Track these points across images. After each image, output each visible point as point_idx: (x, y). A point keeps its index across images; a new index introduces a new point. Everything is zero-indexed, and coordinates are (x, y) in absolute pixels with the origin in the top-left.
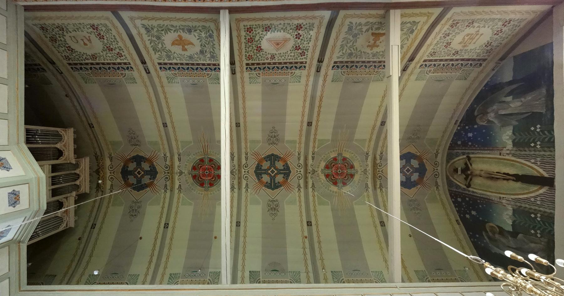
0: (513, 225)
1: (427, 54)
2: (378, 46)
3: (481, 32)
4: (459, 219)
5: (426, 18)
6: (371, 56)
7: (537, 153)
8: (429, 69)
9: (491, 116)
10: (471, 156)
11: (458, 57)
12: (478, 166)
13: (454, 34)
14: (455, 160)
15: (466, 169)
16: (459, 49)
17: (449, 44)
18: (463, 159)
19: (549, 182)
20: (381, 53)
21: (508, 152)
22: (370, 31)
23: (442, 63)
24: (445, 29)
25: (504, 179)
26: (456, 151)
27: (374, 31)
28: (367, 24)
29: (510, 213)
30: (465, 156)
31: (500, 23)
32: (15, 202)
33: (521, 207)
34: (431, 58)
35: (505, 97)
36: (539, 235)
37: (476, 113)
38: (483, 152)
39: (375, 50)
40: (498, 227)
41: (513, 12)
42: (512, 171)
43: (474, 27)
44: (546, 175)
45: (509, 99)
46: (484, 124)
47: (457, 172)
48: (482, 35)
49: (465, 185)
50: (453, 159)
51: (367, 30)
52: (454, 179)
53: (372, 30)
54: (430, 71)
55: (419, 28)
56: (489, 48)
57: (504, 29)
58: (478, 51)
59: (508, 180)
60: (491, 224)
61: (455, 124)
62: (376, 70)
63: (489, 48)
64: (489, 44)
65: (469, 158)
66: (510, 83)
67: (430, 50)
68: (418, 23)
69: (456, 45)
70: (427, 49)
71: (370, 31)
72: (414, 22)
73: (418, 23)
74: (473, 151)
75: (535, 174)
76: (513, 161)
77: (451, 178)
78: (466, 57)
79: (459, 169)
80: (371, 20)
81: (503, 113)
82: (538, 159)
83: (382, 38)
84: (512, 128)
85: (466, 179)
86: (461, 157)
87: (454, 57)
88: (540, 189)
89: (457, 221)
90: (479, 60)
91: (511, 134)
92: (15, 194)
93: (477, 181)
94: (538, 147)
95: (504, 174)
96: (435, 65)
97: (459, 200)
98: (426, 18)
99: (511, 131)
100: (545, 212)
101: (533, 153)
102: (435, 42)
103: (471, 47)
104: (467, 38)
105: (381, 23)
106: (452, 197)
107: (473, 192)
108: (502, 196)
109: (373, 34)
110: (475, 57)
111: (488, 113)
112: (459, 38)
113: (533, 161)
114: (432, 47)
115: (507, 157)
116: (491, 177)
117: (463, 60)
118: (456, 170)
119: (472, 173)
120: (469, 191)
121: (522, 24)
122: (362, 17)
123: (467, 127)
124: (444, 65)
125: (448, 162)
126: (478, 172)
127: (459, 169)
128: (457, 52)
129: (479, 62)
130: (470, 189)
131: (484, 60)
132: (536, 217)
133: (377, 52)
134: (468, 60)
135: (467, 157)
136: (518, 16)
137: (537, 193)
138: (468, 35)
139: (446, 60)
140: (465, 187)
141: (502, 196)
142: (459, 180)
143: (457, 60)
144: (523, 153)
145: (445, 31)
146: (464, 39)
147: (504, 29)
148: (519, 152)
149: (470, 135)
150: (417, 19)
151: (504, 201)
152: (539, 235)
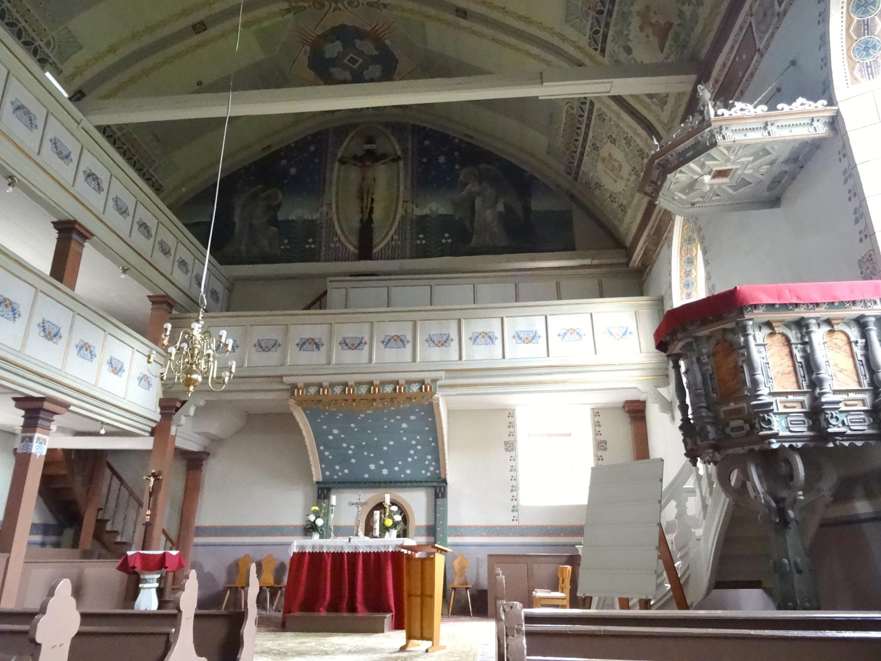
0: (288, 222)
1: (604, 109)
2: (642, 28)
3: (619, 181)
4: (274, 149)
5: (665, 121)
6: (625, 9)
7: (408, 241)
8: (575, 106)
9: (473, 187)
10: (401, 164)
11: (587, 149)
12: (381, 173)
13: (627, 150)
14: (392, 138)
15: (372, 157)
16: (600, 152)
17: (614, 142)
18: (394, 149)
19: (365, 251)
20: (625, 32)
21: (409, 210)
22: (677, 21)
23: (583, 127)
24: (639, 141)
25: (362, 208)
26: (410, 138)
27: (675, 28)
28: (695, 17)
29: (308, 217)
30: (399, 153)
31: (625, 203)
32: (44, 330)
33: (321, 228)
34: (595, 114)
35: (504, 203)
36: (282, 247)
37: (483, 166)
38: (409, 182)
39: (635, 22)
40: (280, 203)
41: (635, 217)
42: (377, 215)
43: (630, 175)
44: (375, 251)
45: (501, 207)
46: (461, 177)
47: (367, 143)
48: (616, 181)
49: (343, 157)
50: (393, 134)
51: (681, 15)
52: (353, 138)
53: (679, 25)
54: (572, 108)
55: (653, 107)
56: (592, 185)
57: (616, 205)
58: (591, 175)
59: (362, 212)
60: (280, 195)
61: (466, 135)
62: (592, 13)
63: (593, 186)
64: (598, 186)
65: (396, 159)
66: (527, 210)
67: (609, 114)
68: (662, 109)
69: (607, 149)
70: (613, 111)
71: (677, 21)
72: (665, 103)
73: (662, 109)
74: (410, 164)
75: (376, 240)
76: (395, 218)
77: (352, 133)
78: (585, 158)
79: (373, 146)
80: (698, 29)
81: (476, 201)
82: (399, 243)
83: (654, 40)
84: (450, 213)
85: (355, 157)
86: (397, 147)
87: (589, 144)
88: (354, 246)
89: (269, 147)
90: (577, 173)
91: (440, 212)
92: (55, 336)
93: (354, 174)
94: (418, 242)
95: (372, 208)
96: (582, 116)
97: (312, 148)
98: (665, 121)
99: (444, 213)
100: (320, 252)
101: (408, 236)
102: (621, 125)
103: (600, 167)
104: (616, 164)
105: (685, 47)
106: (314, 136)
107: (332, 170)
108: (334, 206)
109: (670, 25)
110: (583, 168)
111: (480, 183)
112: (618, 154)
113: (396, 237)
114: (615, 118)
115: (400, 211)
116: (364, 194)
117: (582, 154)
118: (370, 140)
119: (368, 166)
120: (333, 163)
121: (616, 222)
122: (711, 14)
123: (457, 154)
124: (579, 128)
125: (387, 125)
126: (369, 175)
127: (373, 146)
128: (596, 149)
129: (574, 172)
130: (337, 164)
131: (576, 179)
132: (309, 243)
133: (630, 24)
134: (580, 160)
135: (399, 158)
136: (627, 219)
137: (347, 244)
138: (620, 166)
139: (586, 134)
140: (339, 155)
141: (334, 206)
142: (350, 145)
143: (583, 147)
144: (409, 228)
145: (635, 142)
146: (616, 160)
147: (616, 205)
148: (409, 223)
149: (442, 159)
150: (668, 108)
151: (325, 209)
152: (282, 247)
